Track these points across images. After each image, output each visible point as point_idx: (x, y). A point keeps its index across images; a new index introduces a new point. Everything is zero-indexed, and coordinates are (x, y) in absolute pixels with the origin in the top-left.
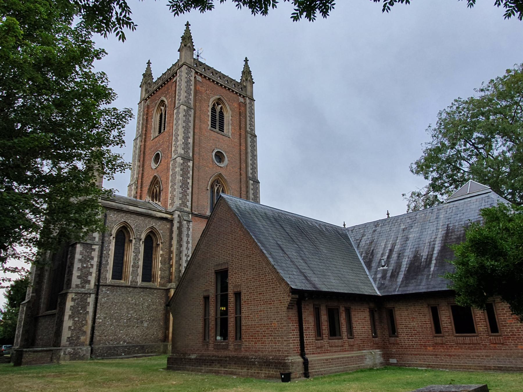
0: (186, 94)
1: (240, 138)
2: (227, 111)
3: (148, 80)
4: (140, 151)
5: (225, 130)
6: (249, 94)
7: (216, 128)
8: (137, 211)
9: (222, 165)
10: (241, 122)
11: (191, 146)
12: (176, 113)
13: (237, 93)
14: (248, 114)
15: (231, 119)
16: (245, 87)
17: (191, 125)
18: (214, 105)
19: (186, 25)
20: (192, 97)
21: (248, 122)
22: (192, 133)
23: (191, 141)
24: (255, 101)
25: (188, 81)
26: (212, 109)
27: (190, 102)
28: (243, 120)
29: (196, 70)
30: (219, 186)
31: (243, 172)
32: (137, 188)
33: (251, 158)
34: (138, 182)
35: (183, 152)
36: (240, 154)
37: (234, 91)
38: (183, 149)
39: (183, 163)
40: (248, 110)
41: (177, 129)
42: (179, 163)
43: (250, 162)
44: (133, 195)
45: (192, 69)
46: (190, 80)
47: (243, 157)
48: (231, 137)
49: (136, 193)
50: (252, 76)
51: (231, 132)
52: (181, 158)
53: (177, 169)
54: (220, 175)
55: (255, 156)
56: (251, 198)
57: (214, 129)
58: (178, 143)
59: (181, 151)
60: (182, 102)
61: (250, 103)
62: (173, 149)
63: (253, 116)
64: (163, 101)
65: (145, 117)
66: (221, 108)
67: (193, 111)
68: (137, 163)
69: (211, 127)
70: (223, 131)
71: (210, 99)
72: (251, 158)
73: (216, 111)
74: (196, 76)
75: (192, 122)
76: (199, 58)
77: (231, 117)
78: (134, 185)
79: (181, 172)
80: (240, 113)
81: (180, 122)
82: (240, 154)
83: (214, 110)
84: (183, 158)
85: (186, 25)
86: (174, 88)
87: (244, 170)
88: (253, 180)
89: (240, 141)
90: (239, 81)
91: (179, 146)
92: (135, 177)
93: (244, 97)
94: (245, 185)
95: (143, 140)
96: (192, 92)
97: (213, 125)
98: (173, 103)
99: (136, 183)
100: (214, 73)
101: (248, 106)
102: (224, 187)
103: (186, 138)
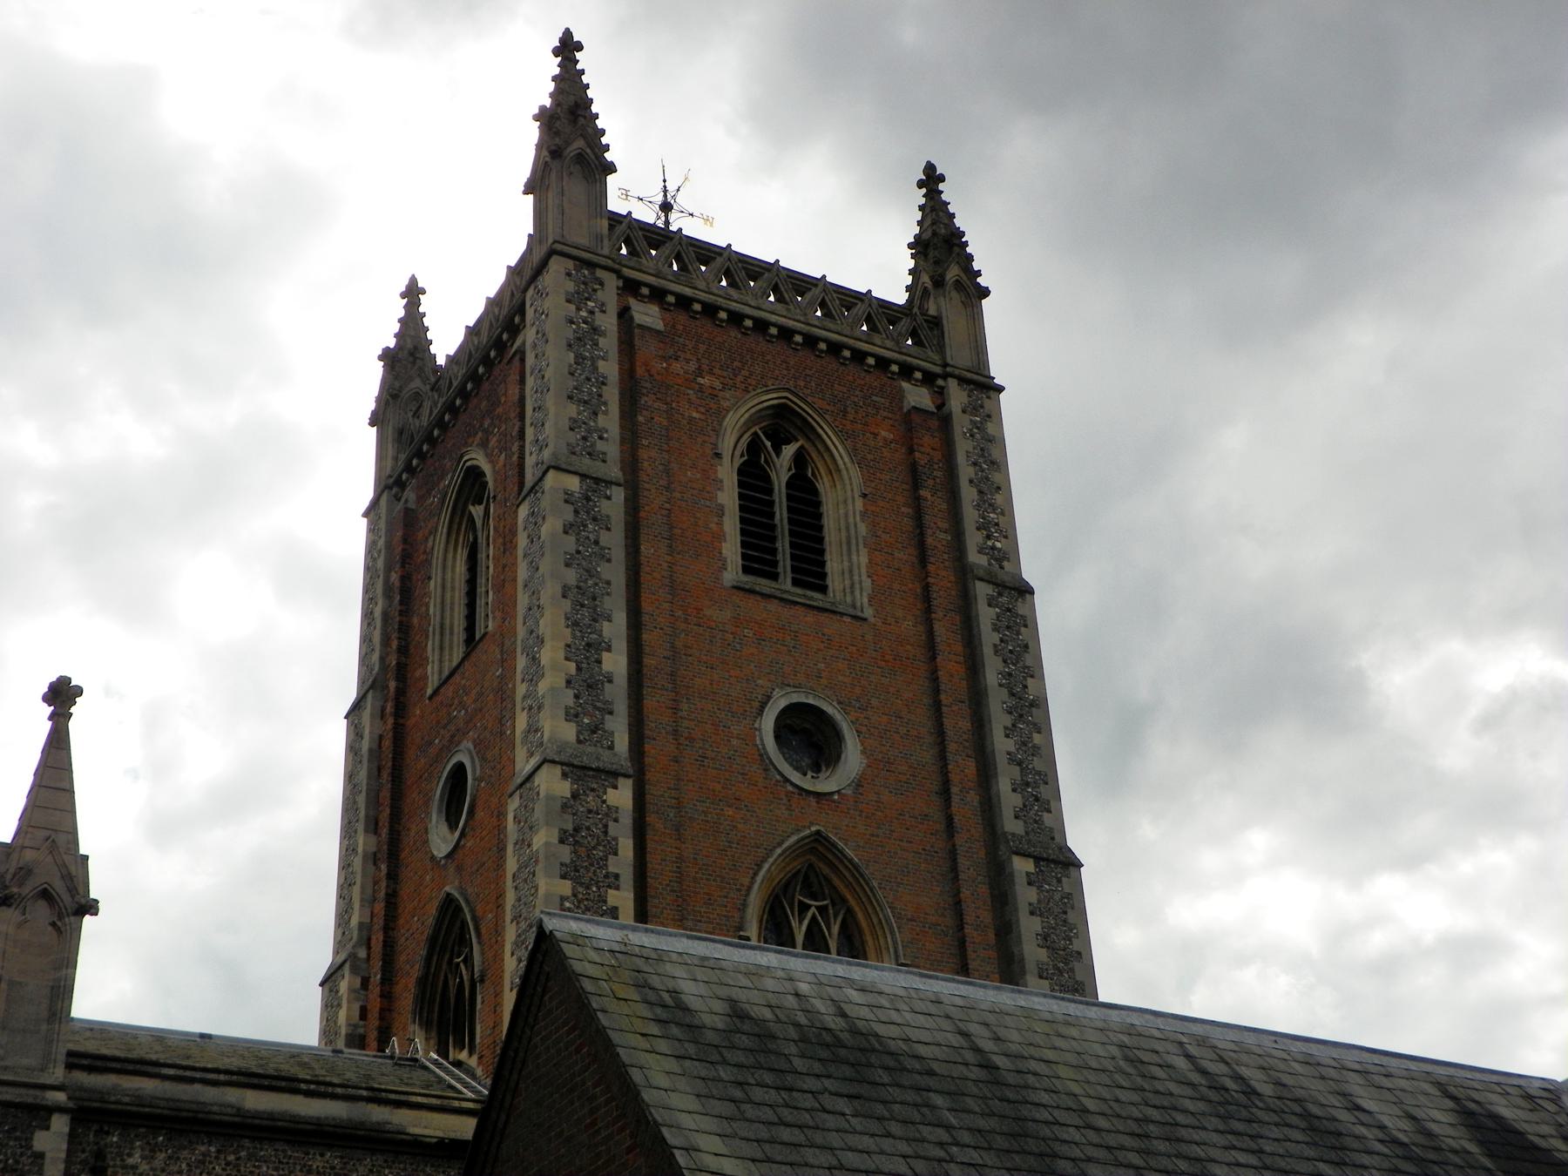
0: (572, 410)
1: (928, 610)
2: (834, 470)
3: (411, 379)
4: (379, 769)
5: (835, 582)
6: (958, 356)
7: (774, 577)
8: (295, 1119)
9: (827, 784)
10: (927, 519)
11: (617, 693)
12: (526, 520)
13: (883, 363)
14: (965, 471)
15: (864, 514)
16: (936, 323)
17: (615, 573)
18: (754, 447)
19: (921, 184)
20: (610, 421)
21: (970, 516)
22: (620, 618)
23: (616, 662)
24: (1000, 389)
25: (584, 339)
26: (740, 472)
27: (600, 446)
28: (934, 502)
29: (626, 272)
30: (822, 910)
31: (966, 805)
32: (365, 983)
33: (1007, 720)
34: (369, 948)
35: (569, 732)
36: (937, 706)
37: (866, 354)
38: (572, 716)
39: (575, 796)
40: (963, 447)
41: (535, 608)
42: (550, 798)
43: (1002, 744)
44: (343, 1031)
45: (600, 273)
46: (595, 330)
47: (958, 724)
48: (868, 613)
49: (364, 1013)
50: (970, 258)
51: (867, 583)
52: (558, 770)
53: (542, 839)
54: (818, 844)
55: (1033, 704)
56: (1031, 966)
57: (764, 584)
58: (543, 687)
59: (559, 730)
60: (554, 455)
61: (973, 408)
62: (521, 722)
63: (996, 477)
64: (474, 474)
65: (395, 577)
66: (800, 460)
67: (618, 494)
68: (361, 839)
69: (746, 570)
70: (823, 589)
71: (721, 414)
72: (1007, 720)
73: (768, 479)
74: (632, 302)
75: (618, 553)
76: (673, 216)
77: (859, 503)
78: (347, 970)
79: (565, 853)
80: (914, 469)
81: (545, 566)
82: (937, 706)
83: (753, 476)
84: (573, 769)
85: (921, 184)
86: (514, 391)
87: (973, 798)
88: (1038, 851)
89: (930, 633)
90: (901, 298)
91: (547, 702)
92: (355, 921)
93: (929, 379)
94: (984, 889)
95: (389, 708)
96: (612, 394)
97: (758, 559)
98: (512, 473)
99: (362, 954)
100: (834, 305)
101: (961, 423)
102: (850, 911)
103: (587, 650)
